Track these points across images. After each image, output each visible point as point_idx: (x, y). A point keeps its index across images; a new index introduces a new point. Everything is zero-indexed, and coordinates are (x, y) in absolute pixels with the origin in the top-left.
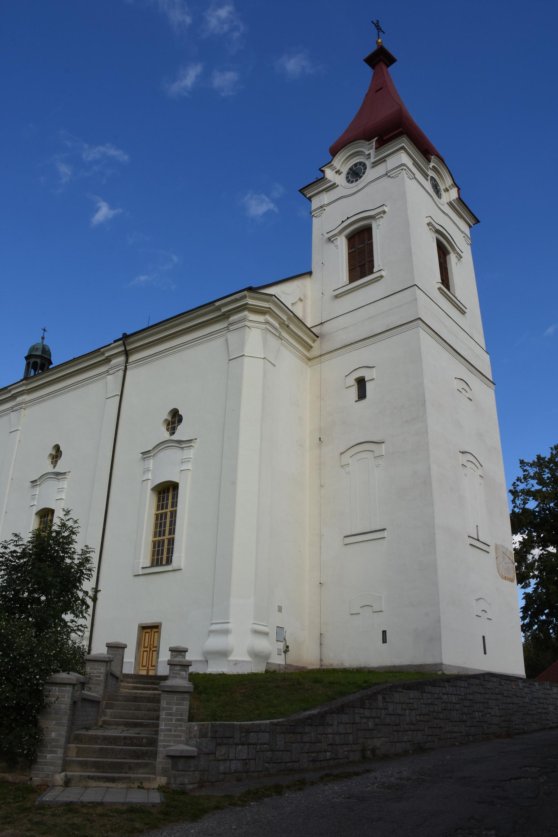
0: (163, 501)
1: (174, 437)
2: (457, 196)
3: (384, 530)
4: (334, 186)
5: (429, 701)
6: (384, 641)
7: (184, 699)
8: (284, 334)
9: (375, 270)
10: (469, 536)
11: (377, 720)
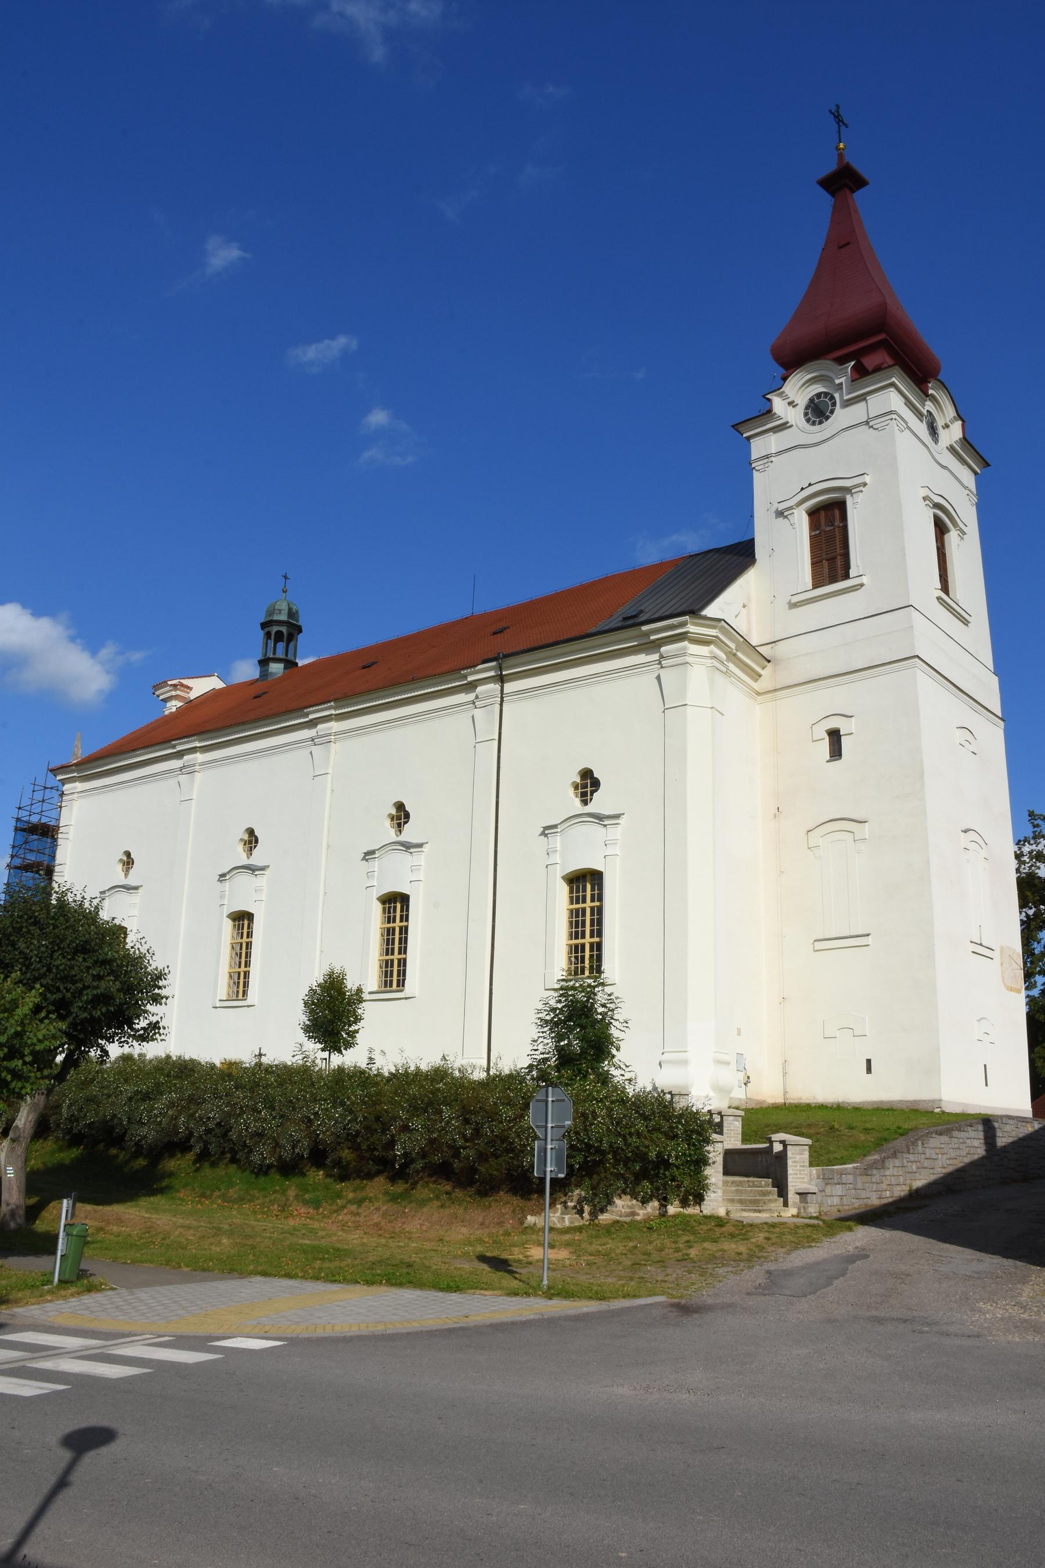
0: (578, 891)
1: (590, 808)
2: (961, 436)
3: (868, 935)
4: (784, 426)
5: (956, 1146)
6: (869, 1070)
7: (804, 1150)
8: (732, 667)
9: (853, 572)
10: (971, 942)
11: (918, 1164)
